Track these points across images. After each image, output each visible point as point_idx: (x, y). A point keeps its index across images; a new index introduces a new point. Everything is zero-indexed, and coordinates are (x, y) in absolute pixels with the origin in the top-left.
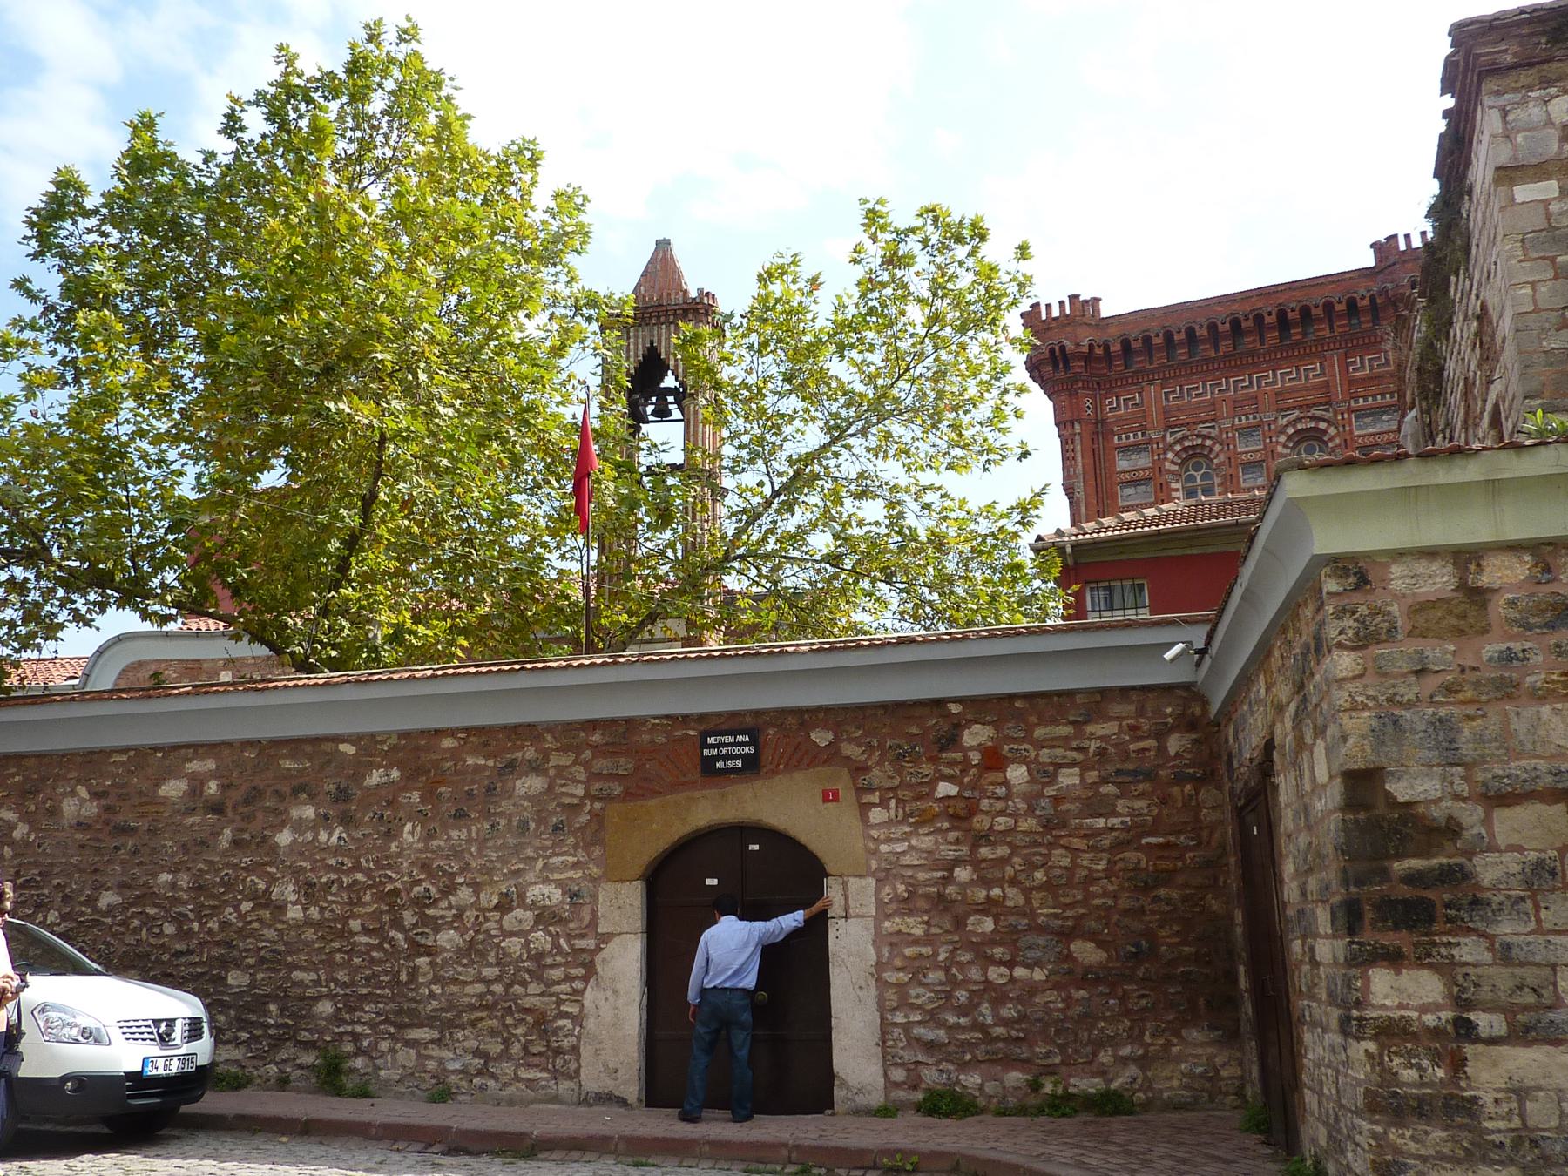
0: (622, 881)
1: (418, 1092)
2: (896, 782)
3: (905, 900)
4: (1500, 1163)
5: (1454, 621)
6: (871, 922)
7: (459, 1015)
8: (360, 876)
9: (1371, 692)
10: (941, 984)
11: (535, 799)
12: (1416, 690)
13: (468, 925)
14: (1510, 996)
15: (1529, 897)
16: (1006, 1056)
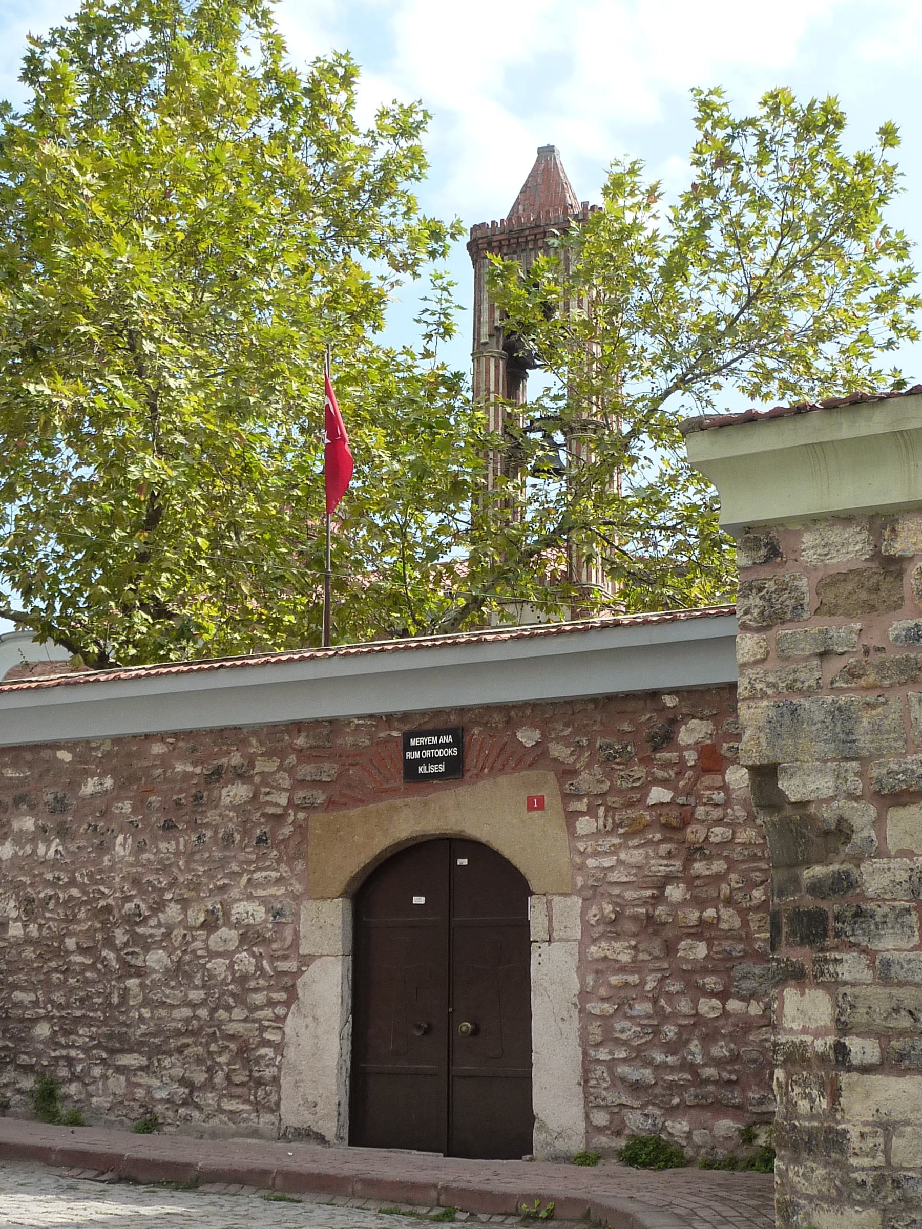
0: (324, 898)
1: (126, 1121)
2: (605, 787)
3: (612, 922)
4: (861, 1203)
5: (864, 595)
6: (575, 946)
7: (166, 1041)
8: (75, 892)
9: (771, 679)
10: (649, 1017)
11: (239, 809)
12: (817, 675)
13: (177, 945)
14: (886, 1018)
15: (915, 909)
16: (717, 1101)
